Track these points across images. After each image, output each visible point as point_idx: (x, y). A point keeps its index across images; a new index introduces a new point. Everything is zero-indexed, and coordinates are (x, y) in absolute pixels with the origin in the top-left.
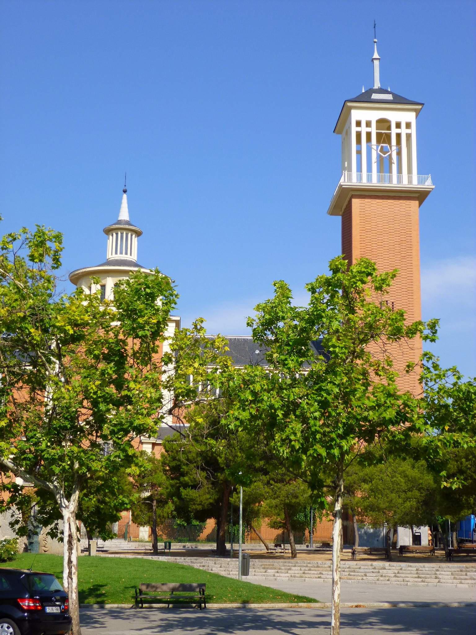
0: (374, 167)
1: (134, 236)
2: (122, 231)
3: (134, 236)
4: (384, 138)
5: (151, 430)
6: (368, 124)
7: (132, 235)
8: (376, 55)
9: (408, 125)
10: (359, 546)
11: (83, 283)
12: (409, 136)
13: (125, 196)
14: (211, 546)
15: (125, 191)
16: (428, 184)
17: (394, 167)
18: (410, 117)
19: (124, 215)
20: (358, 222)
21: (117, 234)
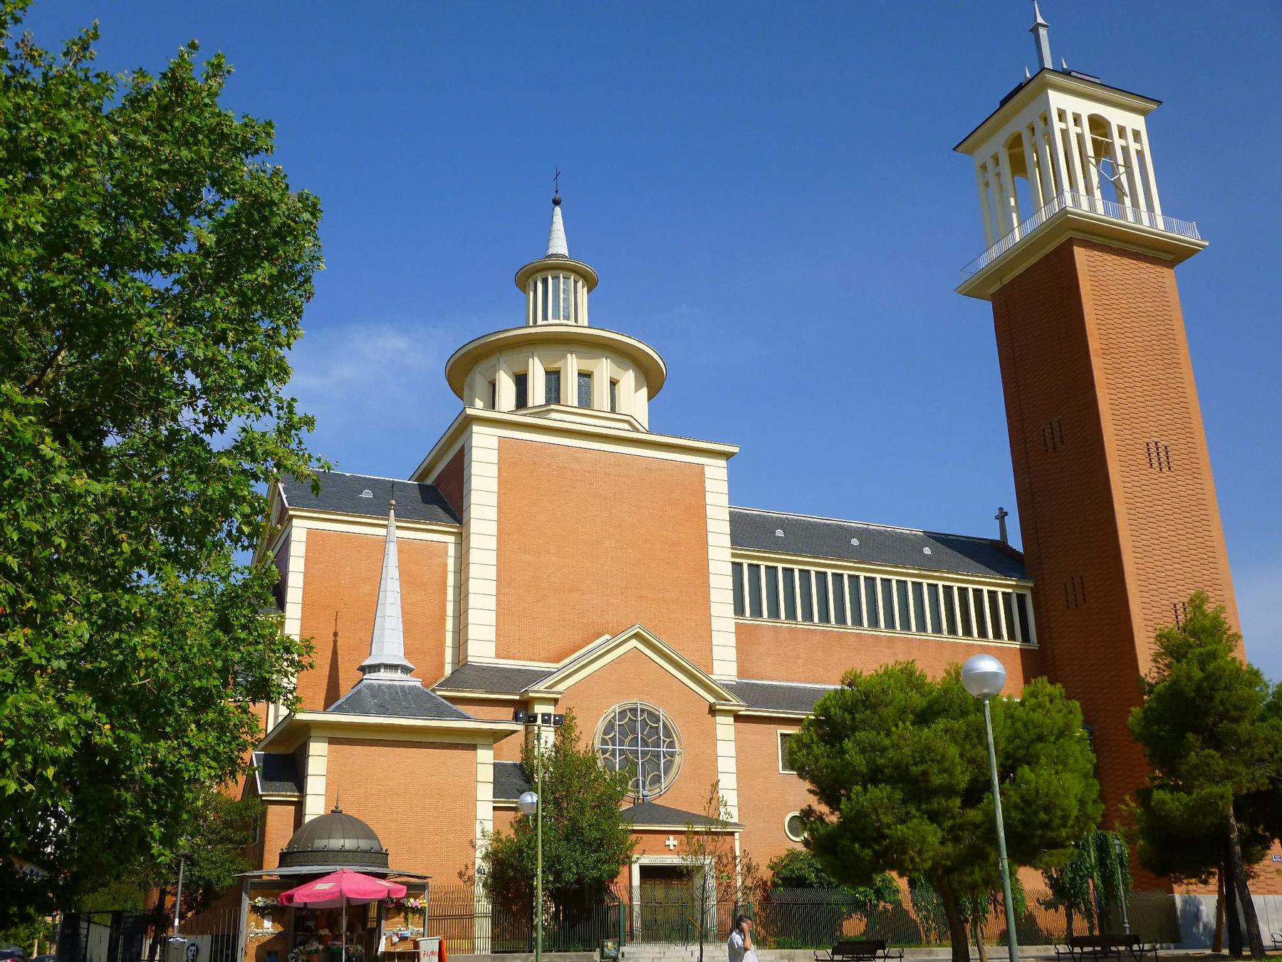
0: (1097, 193)
1: (580, 284)
2: (555, 272)
3: (580, 284)
4: (1103, 149)
5: (863, 702)
6: (1077, 119)
7: (576, 282)
8: (1040, 20)
9: (1137, 135)
10: (311, 532)
11: (502, 364)
12: (1140, 154)
13: (558, 210)
14: (1046, 950)
15: (556, 203)
16: (1189, 235)
17: (1127, 201)
18: (1136, 122)
19: (559, 245)
20: (1089, 288)
21: (545, 282)
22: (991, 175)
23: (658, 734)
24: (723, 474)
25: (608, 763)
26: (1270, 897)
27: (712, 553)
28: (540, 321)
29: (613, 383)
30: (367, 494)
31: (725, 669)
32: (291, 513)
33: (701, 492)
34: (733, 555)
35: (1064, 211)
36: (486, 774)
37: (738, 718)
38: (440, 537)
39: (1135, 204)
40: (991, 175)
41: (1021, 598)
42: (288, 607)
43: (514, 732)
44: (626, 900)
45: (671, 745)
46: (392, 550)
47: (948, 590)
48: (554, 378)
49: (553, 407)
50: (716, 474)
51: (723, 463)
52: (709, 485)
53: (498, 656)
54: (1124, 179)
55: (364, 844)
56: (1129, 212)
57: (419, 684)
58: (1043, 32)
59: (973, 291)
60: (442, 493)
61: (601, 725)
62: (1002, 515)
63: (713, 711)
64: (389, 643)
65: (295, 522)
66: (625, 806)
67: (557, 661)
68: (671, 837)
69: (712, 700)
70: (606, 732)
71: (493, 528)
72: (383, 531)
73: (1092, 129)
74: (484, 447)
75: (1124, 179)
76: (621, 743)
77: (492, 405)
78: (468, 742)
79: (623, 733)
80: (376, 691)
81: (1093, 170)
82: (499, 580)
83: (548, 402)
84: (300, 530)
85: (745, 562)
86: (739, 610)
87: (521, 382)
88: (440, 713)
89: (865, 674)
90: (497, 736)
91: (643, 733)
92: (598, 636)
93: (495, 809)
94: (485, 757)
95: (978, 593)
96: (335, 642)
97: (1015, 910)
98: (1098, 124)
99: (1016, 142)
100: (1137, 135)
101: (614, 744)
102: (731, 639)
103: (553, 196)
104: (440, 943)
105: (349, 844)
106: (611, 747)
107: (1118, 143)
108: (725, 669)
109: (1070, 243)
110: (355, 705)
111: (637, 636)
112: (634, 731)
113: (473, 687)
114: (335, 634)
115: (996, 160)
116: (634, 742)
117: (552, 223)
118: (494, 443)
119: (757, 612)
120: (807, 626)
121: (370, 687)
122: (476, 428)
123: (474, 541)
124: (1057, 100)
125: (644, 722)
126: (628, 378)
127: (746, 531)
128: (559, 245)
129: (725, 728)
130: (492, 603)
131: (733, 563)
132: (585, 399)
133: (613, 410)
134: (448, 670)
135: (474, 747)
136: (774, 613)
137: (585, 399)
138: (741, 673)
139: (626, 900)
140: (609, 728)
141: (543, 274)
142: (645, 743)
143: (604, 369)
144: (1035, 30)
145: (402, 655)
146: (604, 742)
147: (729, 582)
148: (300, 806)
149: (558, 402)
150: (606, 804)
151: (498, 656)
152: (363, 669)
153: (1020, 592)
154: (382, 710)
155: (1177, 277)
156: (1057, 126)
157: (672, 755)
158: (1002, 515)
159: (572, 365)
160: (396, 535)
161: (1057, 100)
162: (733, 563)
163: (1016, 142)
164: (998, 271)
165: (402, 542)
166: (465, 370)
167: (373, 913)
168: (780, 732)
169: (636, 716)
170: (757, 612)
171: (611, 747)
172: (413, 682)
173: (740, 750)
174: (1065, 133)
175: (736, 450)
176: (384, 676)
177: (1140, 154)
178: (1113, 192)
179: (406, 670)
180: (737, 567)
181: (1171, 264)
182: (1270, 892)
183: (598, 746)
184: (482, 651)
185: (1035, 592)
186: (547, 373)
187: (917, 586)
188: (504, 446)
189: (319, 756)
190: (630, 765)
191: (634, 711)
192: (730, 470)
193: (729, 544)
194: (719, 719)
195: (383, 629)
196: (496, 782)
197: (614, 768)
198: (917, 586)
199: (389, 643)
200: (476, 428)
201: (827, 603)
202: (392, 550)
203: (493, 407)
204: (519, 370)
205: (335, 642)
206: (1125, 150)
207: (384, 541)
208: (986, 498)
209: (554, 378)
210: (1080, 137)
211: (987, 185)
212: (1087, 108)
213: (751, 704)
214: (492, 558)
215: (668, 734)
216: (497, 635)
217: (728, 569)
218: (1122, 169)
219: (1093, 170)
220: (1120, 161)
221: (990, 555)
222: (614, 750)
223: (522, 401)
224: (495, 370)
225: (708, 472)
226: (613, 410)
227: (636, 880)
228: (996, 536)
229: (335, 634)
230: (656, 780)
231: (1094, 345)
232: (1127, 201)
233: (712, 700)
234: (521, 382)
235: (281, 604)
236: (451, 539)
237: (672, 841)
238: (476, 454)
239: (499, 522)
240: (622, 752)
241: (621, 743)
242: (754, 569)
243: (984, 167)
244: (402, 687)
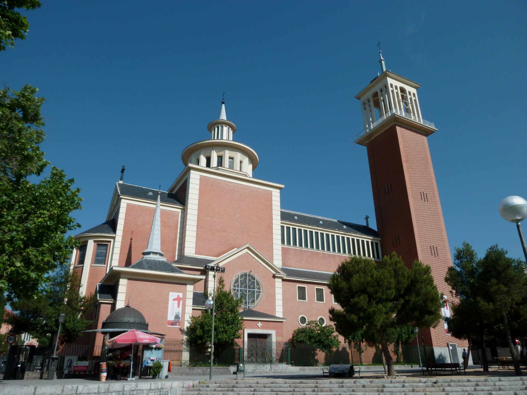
0: (403, 111)
1: (230, 129)
2: (222, 125)
8: (382, 58)
9: (414, 94)
10: (128, 205)
11: (202, 153)
12: (415, 100)
13: (223, 105)
15: (223, 103)
16: (432, 127)
17: (412, 114)
18: (414, 91)
19: (223, 116)
21: (218, 128)
22: (367, 106)
23: (254, 284)
24: (279, 195)
25: (236, 296)
27: (274, 222)
28: (216, 138)
29: (241, 162)
30: (151, 194)
31: (278, 262)
32: (121, 197)
33: (271, 200)
34: (282, 223)
35: (394, 114)
36: (190, 296)
37: (284, 280)
38: (176, 209)
39: (414, 115)
40: (367, 106)
41: (377, 244)
42: (117, 231)
43: (201, 279)
44: (242, 346)
45: (259, 288)
46: (158, 214)
47: (353, 240)
48: (220, 159)
49: (220, 167)
50: (276, 195)
51: (279, 191)
52: (273, 198)
53: (196, 254)
54: (411, 107)
55: (138, 320)
56: (412, 117)
57: (165, 260)
58: (383, 62)
59: (360, 142)
60: (178, 196)
61: (234, 279)
62: (367, 218)
63: (274, 277)
64: (155, 245)
65: (122, 200)
66: (241, 311)
67: (218, 256)
68: (260, 323)
69: (274, 273)
70: (235, 283)
71: (196, 207)
72: (154, 206)
73: (401, 92)
74: (195, 178)
75: (411, 107)
77: (198, 163)
78: (184, 282)
79: (242, 284)
80: (148, 262)
81: (401, 104)
82: (198, 226)
83: (218, 166)
84: (124, 203)
85: (285, 226)
86: (283, 242)
87: (209, 160)
88: (173, 270)
90: (194, 281)
91: (248, 282)
92: (233, 248)
93: (193, 309)
94: (190, 288)
95: (363, 241)
96: (131, 242)
98: (403, 90)
99: (376, 95)
100: (414, 94)
101: (238, 287)
102: (280, 252)
103: (222, 101)
104: (169, 363)
105: (132, 320)
106: (237, 288)
107: (409, 97)
108: (278, 262)
109: (395, 126)
110: (139, 265)
111: (248, 248)
112: (245, 282)
113: (186, 263)
114: (131, 239)
115: (369, 101)
117: (221, 109)
118: (199, 178)
119: (289, 243)
120: (306, 249)
121: (146, 260)
122: (192, 171)
123: (189, 211)
124: (390, 81)
125: (249, 280)
126: (246, 160)
127: (284, 216)
128: (223, 116)
129: (278, 283)
130: (195, 234)
131: (281, 226)
132: (231, 166)
133: (240, 171)
134: (176, 259)
135: (186, 284)
136: (295, 244)
137: (231, 166)
138: (283, 265)
139: (242, 347)
140: (237, 281)
141: (218, 125)
142: (249, 287)
143: (238, 156)
144: (380, 61)
145: (160, 249)
146: (234, 286)
147: (280, 232)
148: (114, 305)
149: (221, 166)
150: (233, 310)
151: (196, 254)
152: (144, 254)
153: (377, 242)
154: (150, 268)
155: (428, 140)
156: (390, 89)
157: (259, 292)
158: (367, 218)
159: (227, 154)
160: (160, 208)
161: (390, 81)
162: (281, 226)
163: (376, 95)
164: (370, 136)
165: (162, 211)
166: (189, 154)
167: (141, 348)
168: (297, 285)
169: (246, 277)
170: (289, 243)
171: (237, 288)
172: (164, 259)
173: (284, 292)
174: (392, 91)
175: (283, 186)
176: (152, 257)
177: (415, 100)
178: (407, 111)
179: (161, 255)
180: (282, 227)
181: (426, 135)
183: (232, 287)
184: (190, 251)
185: (381, 242)
186: (218, 157)
187: (343, 238)
188: (202, 179)
189: (123, 284)
190: (243, 296)
191: (246, 275)
192: (281, 193)
193: (280, 219)
194: (276, 280)
195: (153, 239)
196: (194, 299)
197: (238, 296)
198: (343, 238)
199: (155, 245)
200: (192, 171)
201: (312, 241)
202: (158, 214)
203: (198, 164)
204: (208, 155)
205: (131, 242)
206: (411, 99)
207: (155, 210)
208: (365, 211)
209: (220, 159)
210: (397, 93)
211: (365, 109)
212: (399, 85)
213: (288, 275)
214: (196, 218)
215: (258, 284)
216: (196, 246)
217: (280, 228)
218: (410, 105)
219: (401, 104)
220: (409, 102)
221: (365, 230)
222: (238, 290)
223: (208, 165)
224: (199, 154)
225: (273, 194)
226: (240, 171)
228: (365, 224)
229: (131, 239)
230: (253, 301)
231: (403, 159)
232: (412, 114)
233: (274, 273)
234: (209, 160)
235: (114, 230)
236: (180, 211)
237: (260, 324)
238: (191, 181)
239: (199, 206)
240: (241, 290)
241: (241, 287)
242: (288, 228)
243: (364, 104)
244: (159, 261)
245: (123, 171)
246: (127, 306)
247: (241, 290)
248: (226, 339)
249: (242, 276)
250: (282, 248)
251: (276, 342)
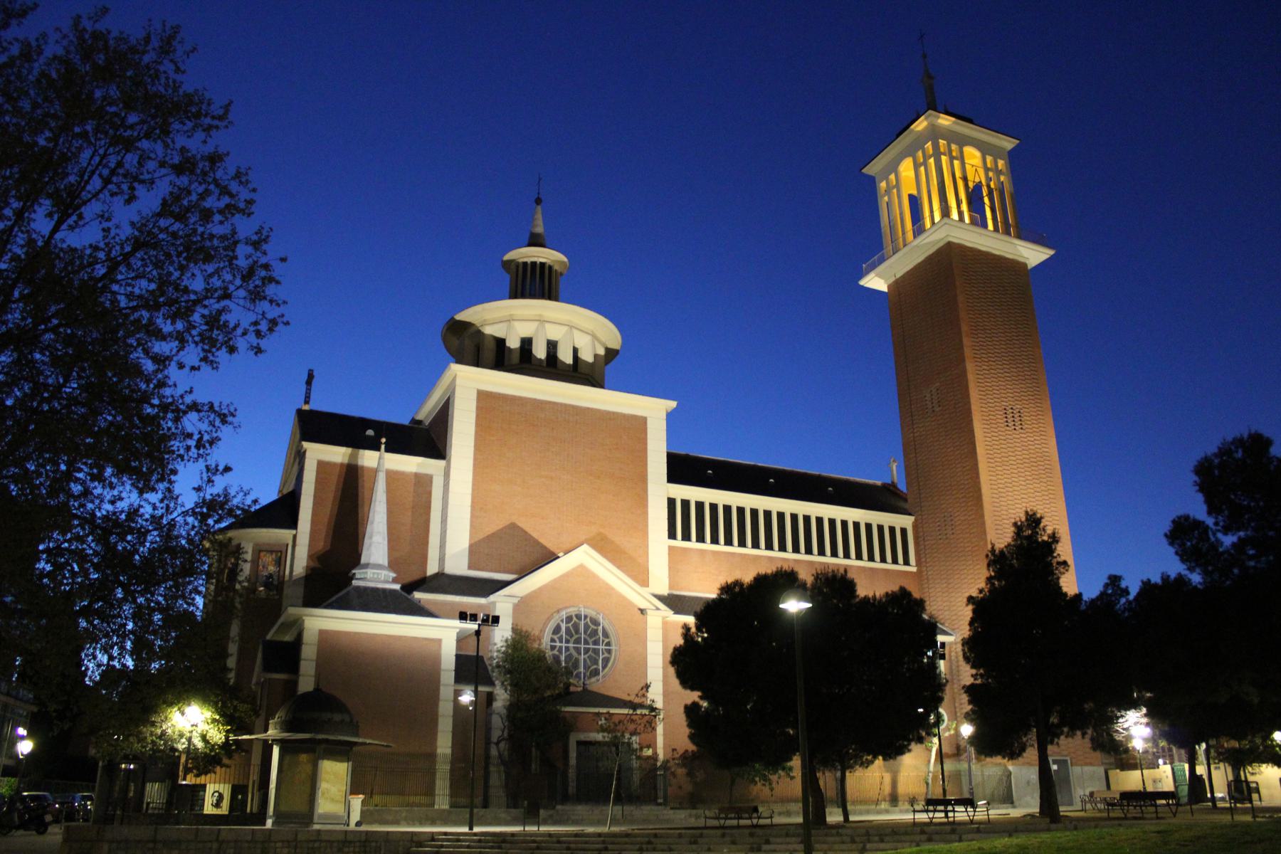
0: (964, 207)
13: (539, 208)
15: (538, 201)
26: (1086, 768)
45: (608, 644)
53: (470, 568)
76: (567, 641)
86: (672, 535)
89: (878, 595)
97: (327, 741)
101: (567, 648)
106: (558, 644)
112: (577, 631)
116: (578, 641)
127: (681, 469)
138: (671, 587)
140: (557, 630)
142: (586, 642)
146: (553, 640)
151: (470, 568)
180: (671, 502)
182: (1086, 764)
215: (606, 634)
227: (573, 755)
240: (587, 651)
245: (309, 382)
246: (317, 690)
247: (567, 648)
248: (204, 738)
249: (569, 619)
250: (670, 548)
251: (459, 658)
